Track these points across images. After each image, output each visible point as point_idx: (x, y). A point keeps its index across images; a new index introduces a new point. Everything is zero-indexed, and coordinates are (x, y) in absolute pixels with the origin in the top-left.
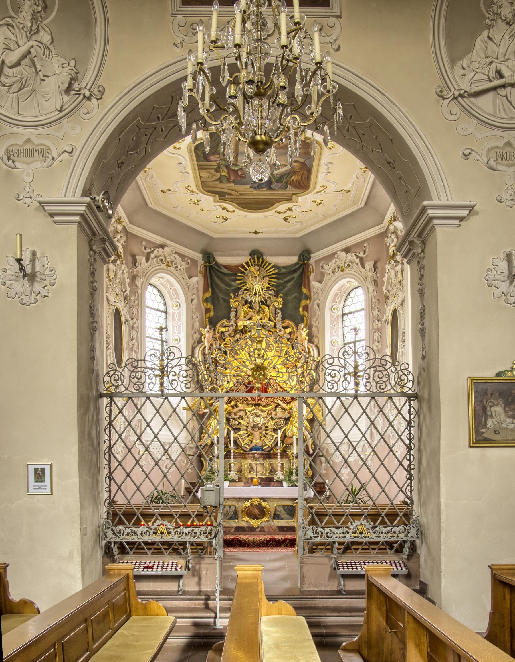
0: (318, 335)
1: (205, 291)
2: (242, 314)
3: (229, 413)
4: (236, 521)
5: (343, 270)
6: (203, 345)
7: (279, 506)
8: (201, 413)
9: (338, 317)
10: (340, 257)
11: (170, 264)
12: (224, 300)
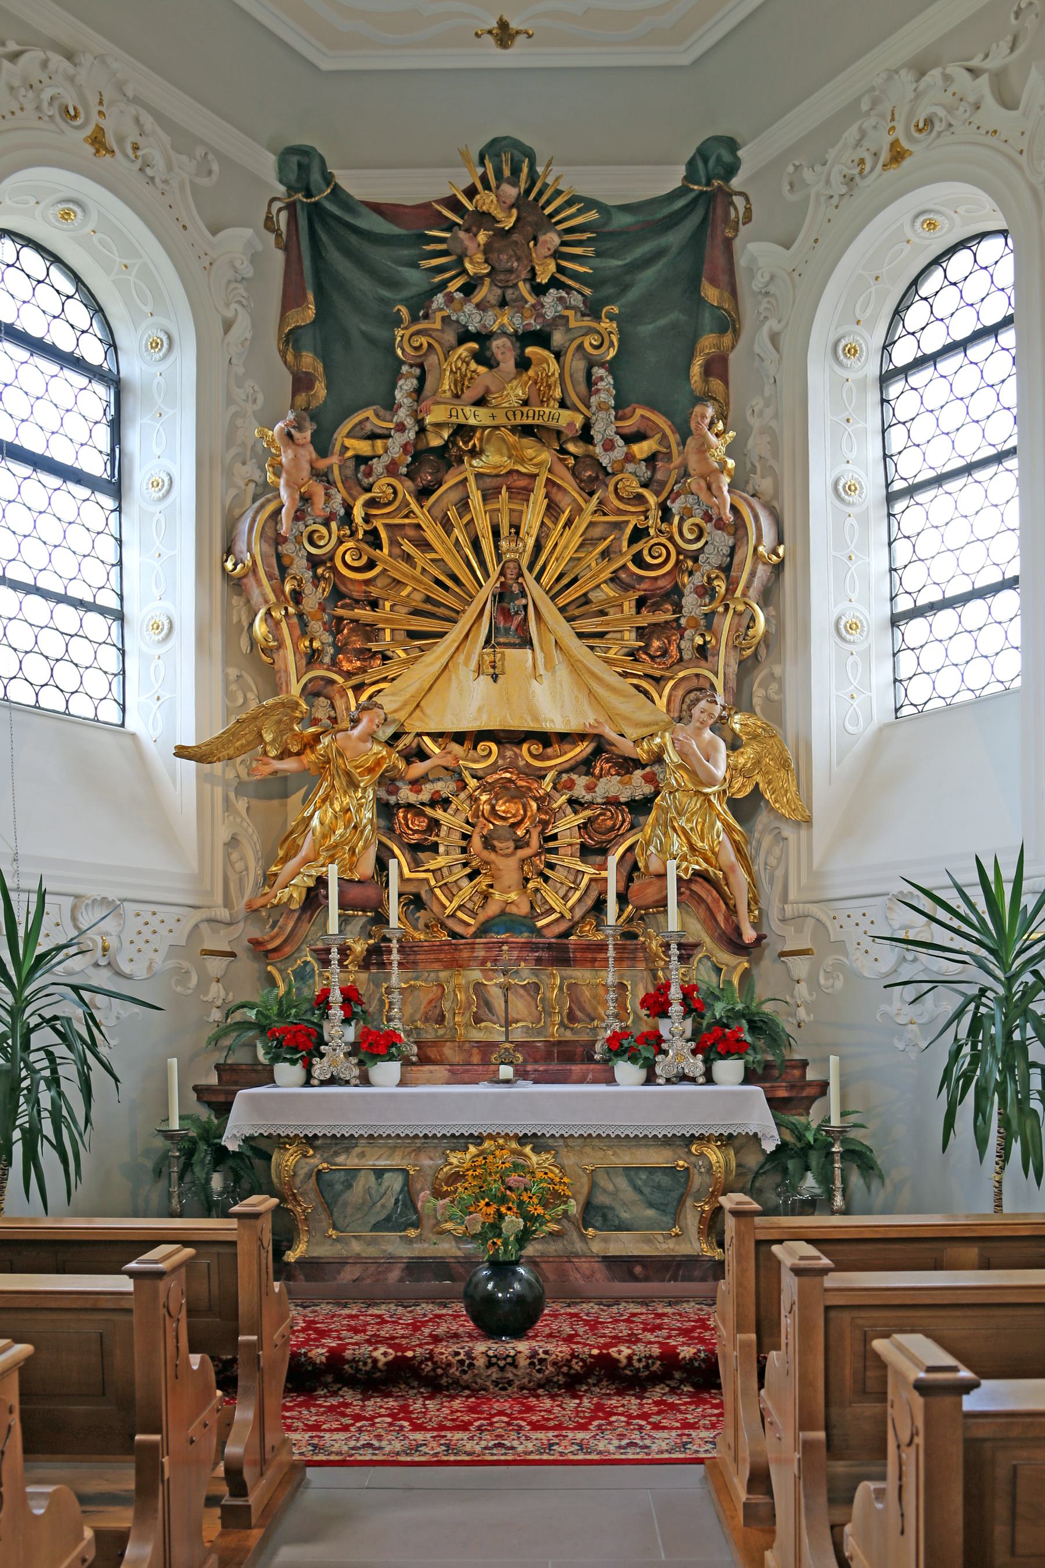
1: (290, 300)
3: (389, 781)
4: (412, 1233)
6: (269, 501)
7: (609, 1171)
12: (372, 341)
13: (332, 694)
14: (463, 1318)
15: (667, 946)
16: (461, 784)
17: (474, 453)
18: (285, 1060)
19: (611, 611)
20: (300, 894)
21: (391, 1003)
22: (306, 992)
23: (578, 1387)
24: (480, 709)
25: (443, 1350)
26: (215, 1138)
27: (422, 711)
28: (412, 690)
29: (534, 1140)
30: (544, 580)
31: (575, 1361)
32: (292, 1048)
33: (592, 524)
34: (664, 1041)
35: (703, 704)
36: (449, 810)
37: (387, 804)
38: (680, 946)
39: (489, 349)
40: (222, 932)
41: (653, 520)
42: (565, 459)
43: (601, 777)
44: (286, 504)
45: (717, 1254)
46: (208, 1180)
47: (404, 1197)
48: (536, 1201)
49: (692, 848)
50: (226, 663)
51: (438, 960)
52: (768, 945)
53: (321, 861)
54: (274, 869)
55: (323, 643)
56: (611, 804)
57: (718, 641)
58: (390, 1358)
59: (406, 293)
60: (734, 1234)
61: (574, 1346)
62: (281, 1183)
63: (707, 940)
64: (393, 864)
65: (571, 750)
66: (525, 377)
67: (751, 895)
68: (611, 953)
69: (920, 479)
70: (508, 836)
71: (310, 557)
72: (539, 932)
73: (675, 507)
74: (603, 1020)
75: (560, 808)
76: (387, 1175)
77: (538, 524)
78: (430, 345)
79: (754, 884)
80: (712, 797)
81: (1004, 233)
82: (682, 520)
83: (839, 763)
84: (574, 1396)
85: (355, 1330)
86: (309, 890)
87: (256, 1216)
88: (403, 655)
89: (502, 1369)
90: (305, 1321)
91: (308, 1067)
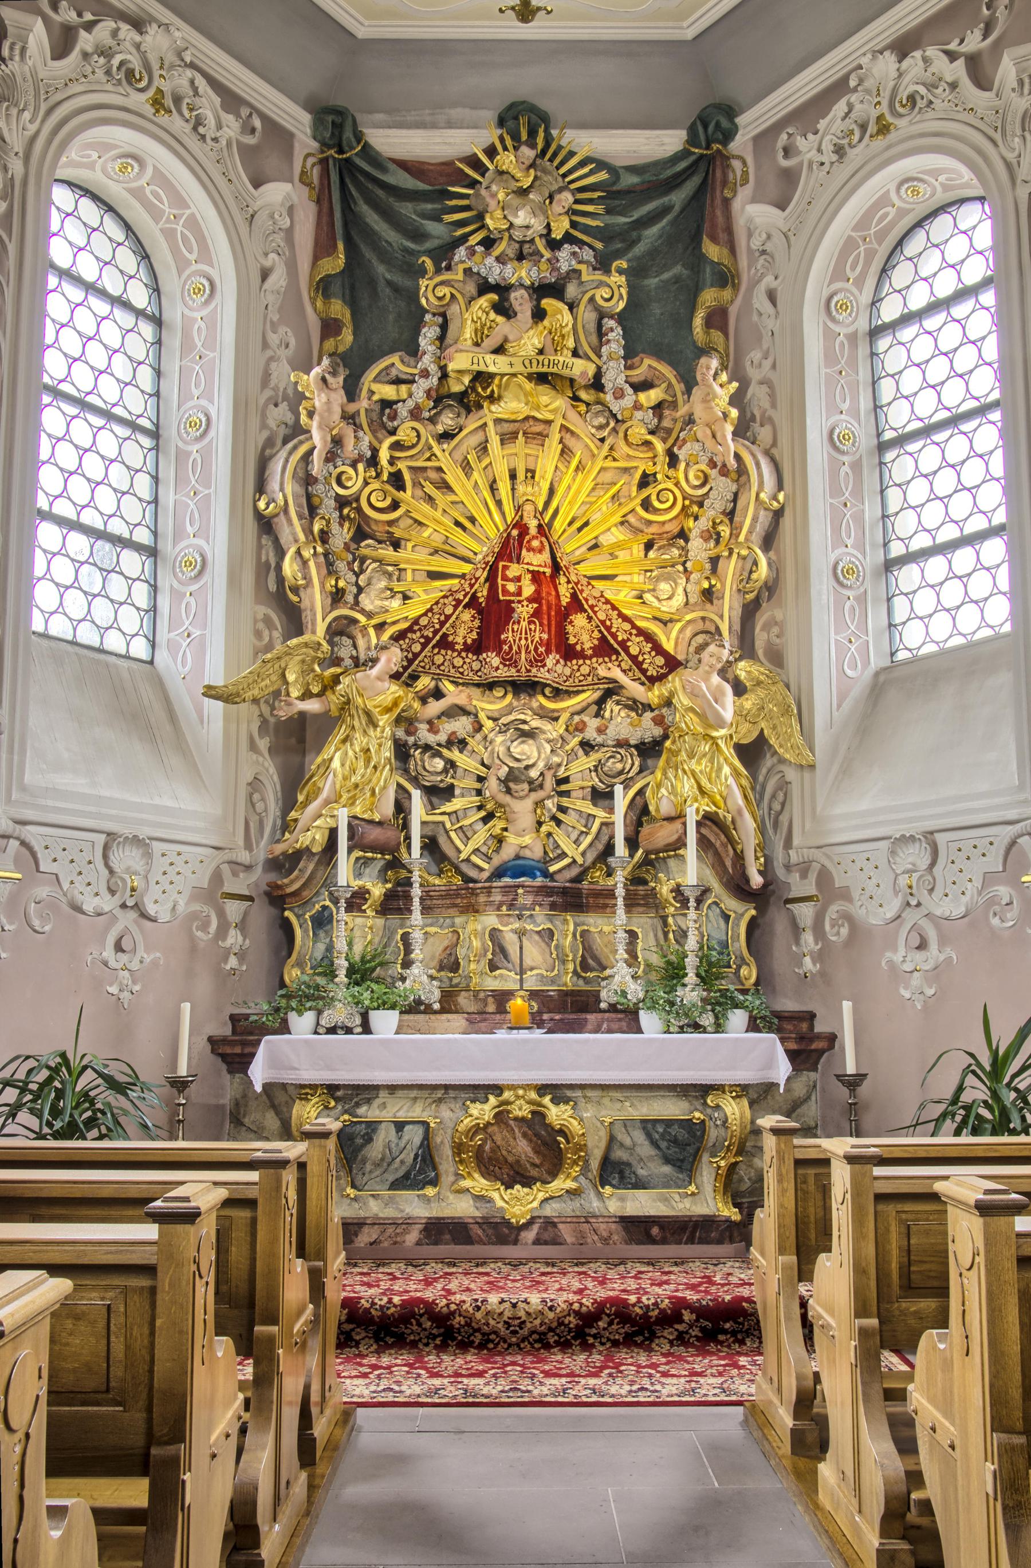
0: (771, 412)
1: (322, 248)
2: (468, 333)
3: (406, 721)
4: (430, 1191)
5: (884, 129)
6: (301, 443)
7: (626, 1123)
8: (283, 713)
9: (853, 338)
10: (868, 84)
11: (168, 102)
17: (492, 399)
35: (712, 648)
39: (507, 299)
41: (661, 467)
51: (455, 905)
52: (774, 892)
57: (723, 585)
59: (429, 245)
60: (774, 1153)
66: (540, 327)
69: (909, 428)
71: (338, 498)
73: (682, 454)
76: (407, 1128)
78: (452, 295)
80: (719, 741)
81: (982, 199)
83: (839, 706)
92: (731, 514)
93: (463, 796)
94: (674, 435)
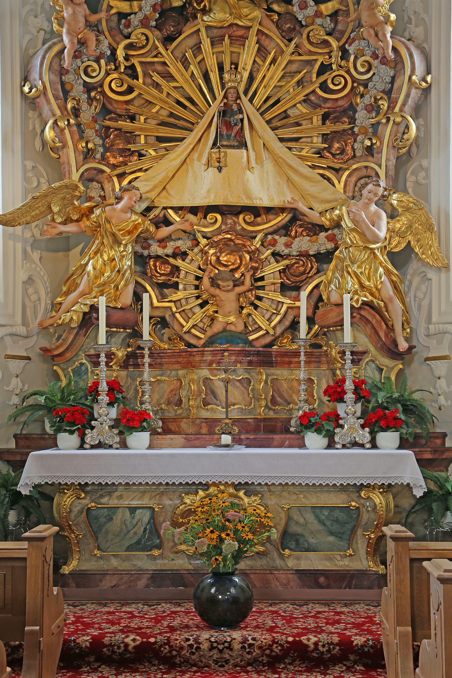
4: (156, 552)
6: (55, 44)
7: (300, 509)
13: (102, 180)
14: (192, 614)
15: (343, 353)
16: (195, 242)
17: (205, 11)
18: (66, 431)
19: (304, 122)
20: (78, 317)
21: (143, 392)
22: (82, 384)
23: (277, 666)
24: (209, 191)
25: (177, 637)
26: (12, 486)
27: (167, 192)
28: (160, 177)
29: (246, 487)
30: (256, 101)
31: (275, 645)
32: (70, 423)
33: (290, 62)
34: (341, 419)
35: (370, 187)
36: (186, 260)
37: (142, 256)
38: (352, 353)
40: (21, 343)
42: (271, 16)
43: (296, 237)
44: (68, 47)
45: (381, 569)
46: (6, 516)
47: (151, 527)
48: (247, 529)
49: (362, 286)
50: (24, 158)
51: (178, 362)
52: (417, 353)
53: (94, 293)
54: (59, 299)
55: (95, 145)
56: (303, 256)
57: (382, 143)
58: (138, 643)
60: (394, 554)
61: (275, 635)
62: (60, 517)
63: (372, 349)
64: (145, 297)
65: (275, 219)
67: (404, 318)
68: (303, 358)
70: (229, 277)
72: (250, 343)
73: (351, 49)
74: (297, 404)
75: (266, 258)
76: (138, 511)
77: (251, 62)
79: (406, 311)
80: (376, 251)
82: (356, 58)
84: (275, 672)
85: (113, 623)
86: (85, 314)
87: (42, 539)
88: (153, 153)
89: (221, 651)
90: (74, 617)
91: (82, 436)
92: (388, 93)
93: (185, 289)
94: (346, 36)
